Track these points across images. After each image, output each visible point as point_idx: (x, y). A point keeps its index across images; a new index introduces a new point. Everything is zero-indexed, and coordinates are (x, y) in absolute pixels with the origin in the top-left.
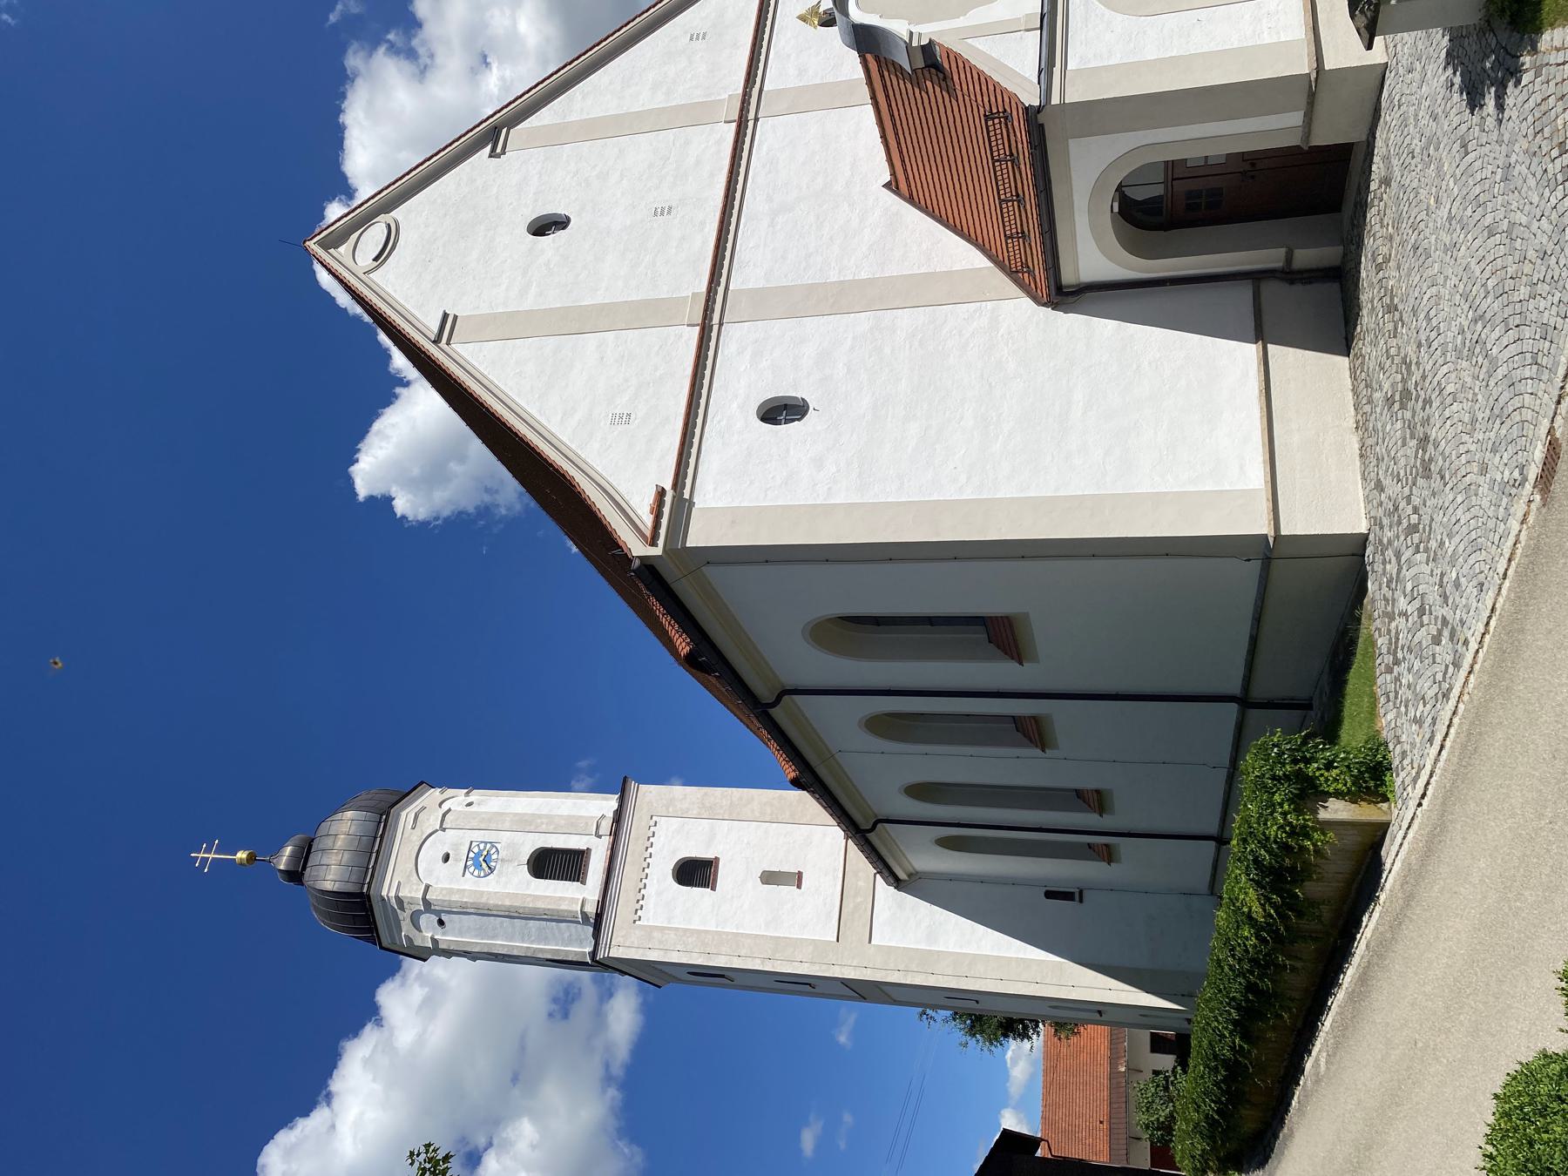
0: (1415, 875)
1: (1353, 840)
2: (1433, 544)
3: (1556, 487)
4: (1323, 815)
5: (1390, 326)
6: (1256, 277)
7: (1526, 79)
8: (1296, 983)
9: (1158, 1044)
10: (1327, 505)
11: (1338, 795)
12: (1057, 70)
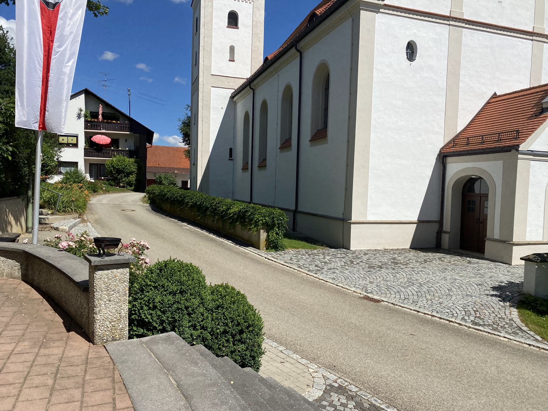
0: (245, 255)
1: (254, 239)
2: (347, 267)
3: (365, 301)
4: (262, 231)
5: (419, 260)
6: (441, 222)
7: (502, 303)
8: (209, 221)
9: (185, 183)
10: (360, 239)
11: (268, 236)
12: (532, 157)
